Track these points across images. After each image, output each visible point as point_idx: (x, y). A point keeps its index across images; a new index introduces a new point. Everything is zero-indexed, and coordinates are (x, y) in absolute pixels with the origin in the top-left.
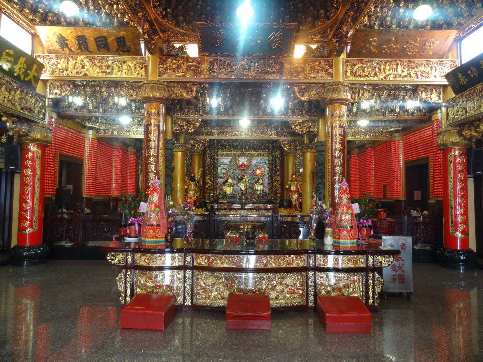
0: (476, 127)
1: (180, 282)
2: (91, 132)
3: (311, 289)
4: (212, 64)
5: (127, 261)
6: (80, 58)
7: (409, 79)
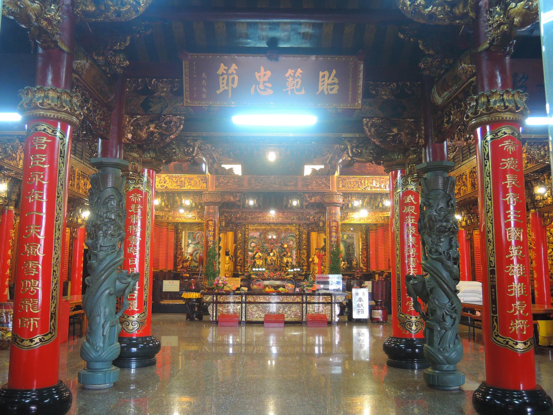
3: (304, 312)
7: (381, 190)
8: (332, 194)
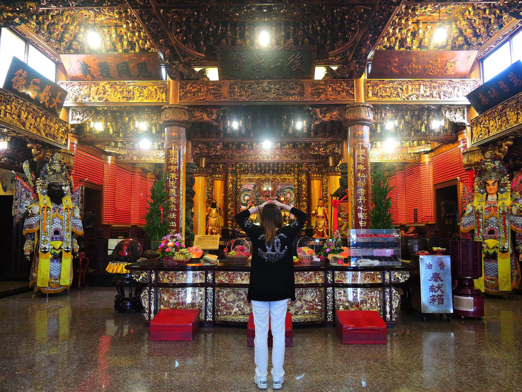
0: (499, 146)
1: (202, 299)
2: (110, 158)
3: (330, 304)
4: (231, 88)
5: (151, 279)
6: (102, 83)
7: (432, 99)
8: (357, 107)
